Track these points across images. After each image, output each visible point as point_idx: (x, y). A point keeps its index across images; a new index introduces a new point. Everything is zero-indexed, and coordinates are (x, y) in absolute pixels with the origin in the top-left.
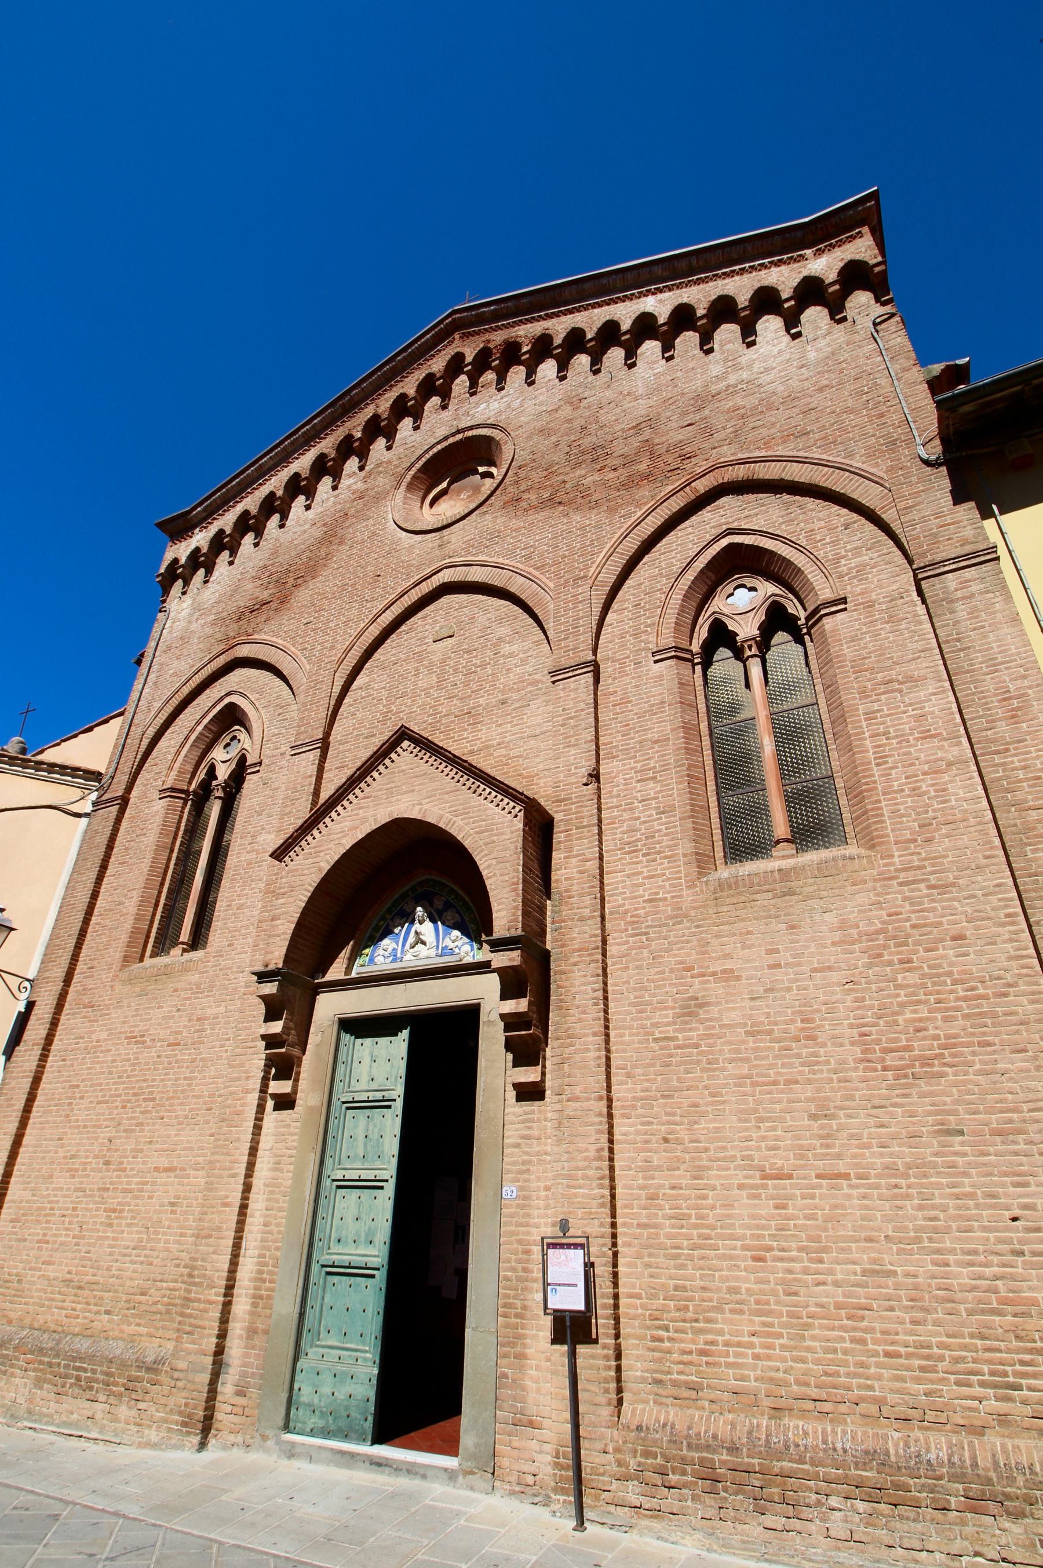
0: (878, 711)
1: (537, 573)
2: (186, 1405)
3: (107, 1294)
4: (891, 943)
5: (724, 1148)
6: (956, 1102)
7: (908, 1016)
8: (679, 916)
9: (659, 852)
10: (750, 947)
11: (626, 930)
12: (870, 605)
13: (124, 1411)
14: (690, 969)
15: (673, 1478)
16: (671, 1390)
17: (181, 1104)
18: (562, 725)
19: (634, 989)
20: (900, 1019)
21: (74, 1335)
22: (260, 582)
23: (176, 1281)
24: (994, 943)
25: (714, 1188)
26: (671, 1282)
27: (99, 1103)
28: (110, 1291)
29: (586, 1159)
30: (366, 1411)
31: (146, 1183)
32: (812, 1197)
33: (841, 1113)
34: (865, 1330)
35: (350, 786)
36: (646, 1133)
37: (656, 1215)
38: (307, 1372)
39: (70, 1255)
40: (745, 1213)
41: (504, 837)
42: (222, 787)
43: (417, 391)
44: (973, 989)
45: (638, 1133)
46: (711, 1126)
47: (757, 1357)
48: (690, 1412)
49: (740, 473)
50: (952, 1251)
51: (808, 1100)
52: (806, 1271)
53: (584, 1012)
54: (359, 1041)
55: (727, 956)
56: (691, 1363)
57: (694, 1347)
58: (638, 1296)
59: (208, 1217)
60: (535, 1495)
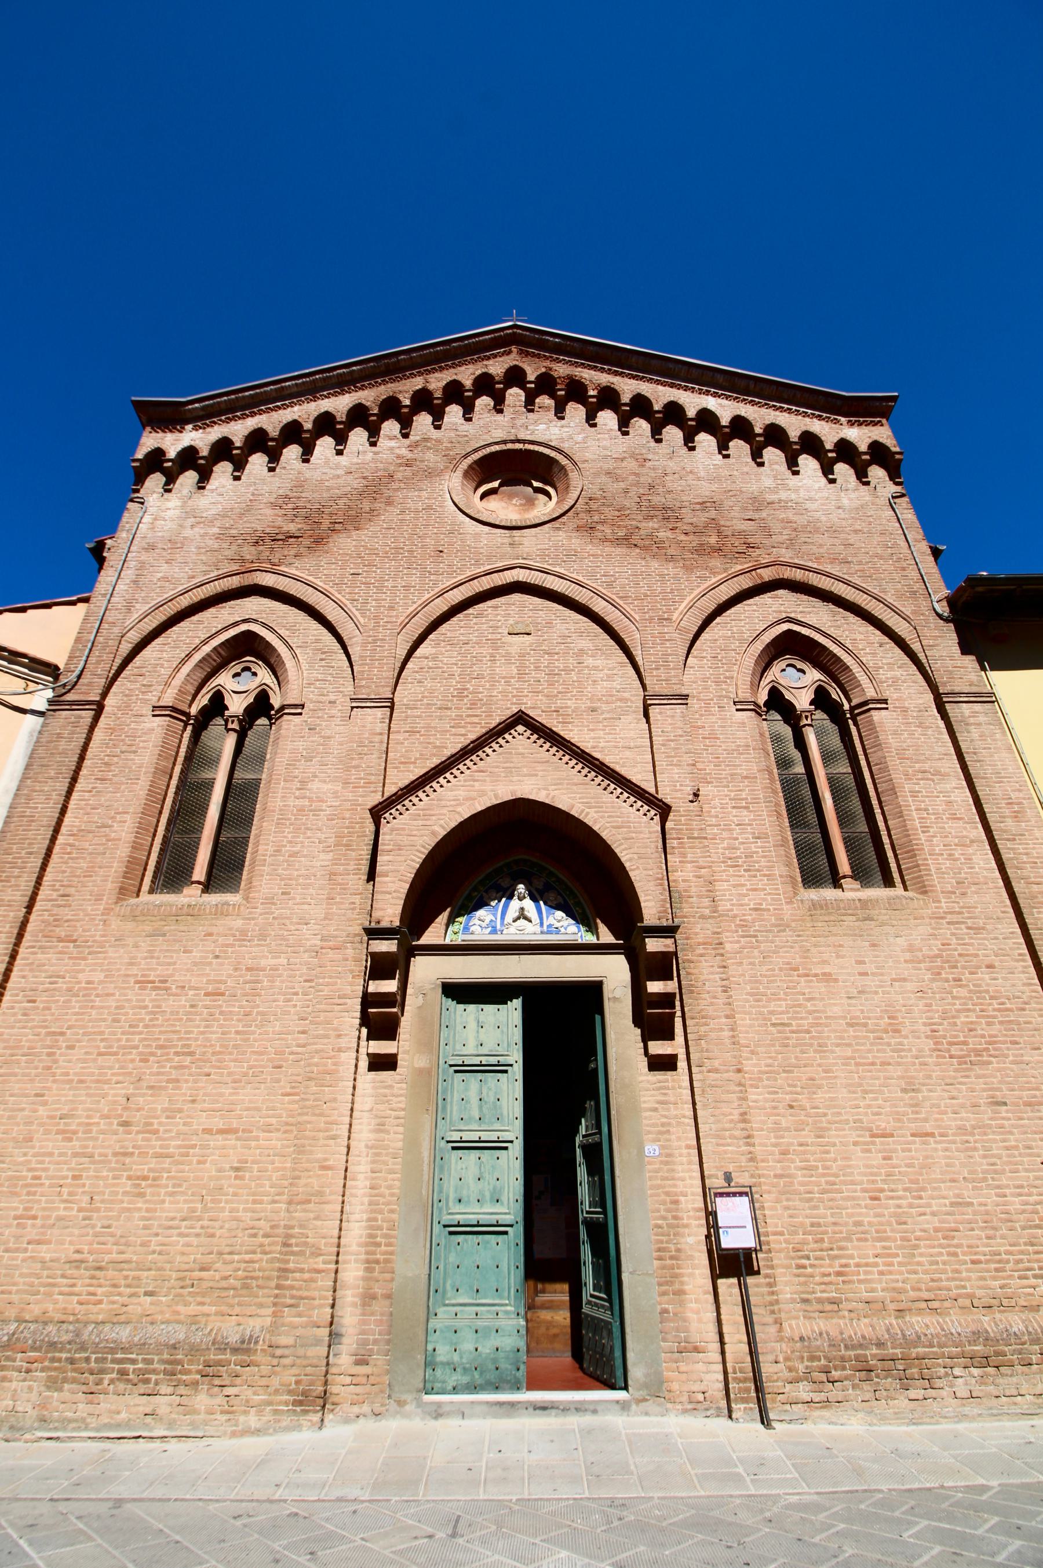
0: (919, 792)
1: (621, 603)
2: (297, 1382)
3: (146, 1273)
4: (946, 965)
5: (839, 1113)
6: (1000, 1082)
7: (962, 1019)
8: (782, 926)
9: (758, 870)
10: (843, 957)
11: (737, 931)
12: (905, 710)
13: (202, 1400)
14: (796, 969)
15: (835, 1374)
16: (817, 1306)
17: (235, 1060)
18: (663, 745)
19: (750, 981)
20: (958, 1021)
21: (97, 1323)
22: (283, 512)
23: (254, 1252)
24: (1013, 973)
25: (834, 1145)
26: (808, 1221)
27: (100, 1054)
28: (150, 1269)
29: (731, 1121)
30: (518, 1361)
31: (194, 1146)
32: (910, 1150)
33: (924, 1088)
34: (957, 1246)
35: (462, 756)
36: (773, 1101)
37: (789, 1167)
38: (442, 1331)
39: (76, 1232)
40: (861, 1163)
41: (642, 835)
42: (239, 720)
43: (473, 385)
44: (1003, 1004)
45: (766, 1100)
46: (827, 1096)
47: (881, 1273)
48: (834, 1321)
49: (798, 575)
50: (1008, 1186)
51: (899, 1078)
52: (911, 1206)
53: (715, 997)
54: (462, 1006)
55: (824, 962)
56: (830, 1283)
57: (831, 1270)
58: (781, 1234)
59: (303, 1181)
60: (707, 1409)
